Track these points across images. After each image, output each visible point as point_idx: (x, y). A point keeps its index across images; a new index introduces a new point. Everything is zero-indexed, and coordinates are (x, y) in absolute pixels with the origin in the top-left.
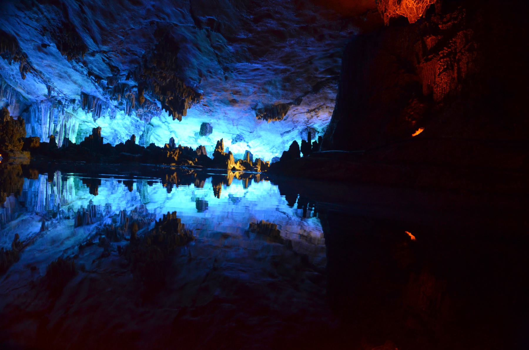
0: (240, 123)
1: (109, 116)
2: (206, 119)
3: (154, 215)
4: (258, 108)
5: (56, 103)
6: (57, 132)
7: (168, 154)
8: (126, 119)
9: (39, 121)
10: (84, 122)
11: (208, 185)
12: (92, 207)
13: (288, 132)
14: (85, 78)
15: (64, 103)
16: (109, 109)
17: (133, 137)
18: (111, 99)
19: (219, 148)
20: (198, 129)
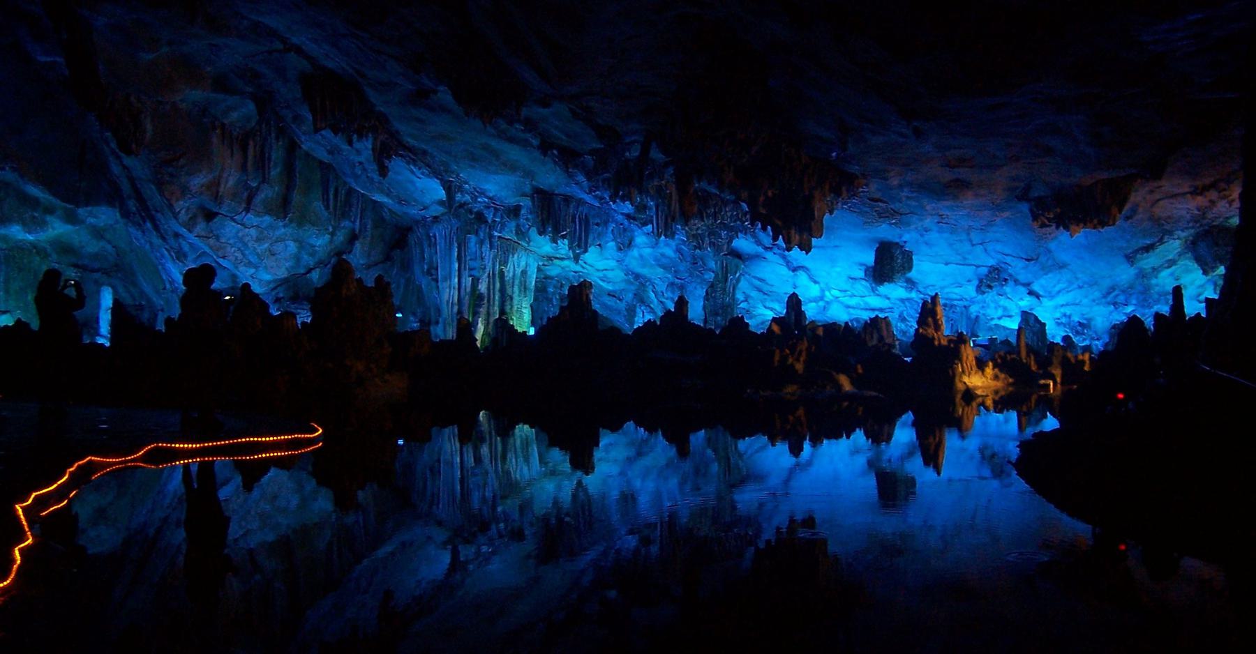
2: (886, 231)
4: (1035, 194)
5: (471, 220)
6: (480, 297)
7: (777, 357)
8: (661, 245)
9: (432, 271)
10: (550, 258)
11: (904, 434)
12: (583, 504)
13: (1148, 249)
14: (537, 154)
15: (490, 217)
16: (612, 226)
17: (682, 303)
18: (613, 198)
19: (928, 326)
20: (870, 259)
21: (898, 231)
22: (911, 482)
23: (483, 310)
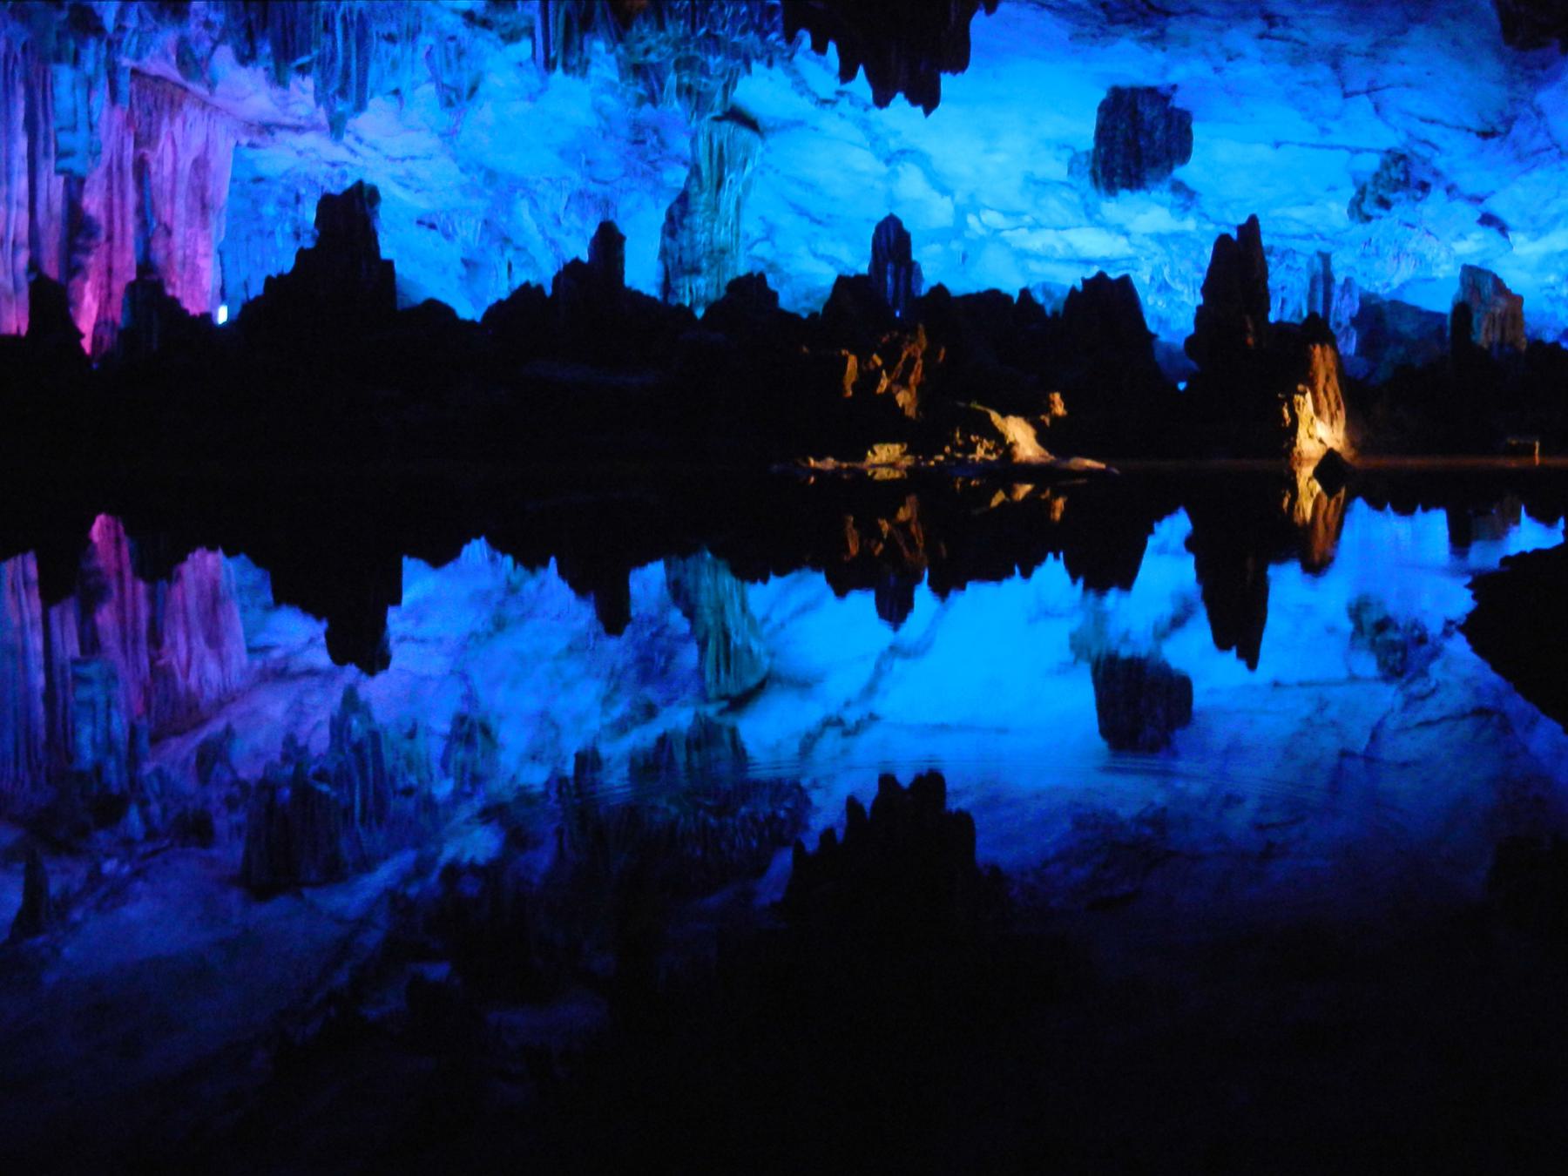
0: (1392, 72)
1: (435, 78)
2: (1132, 62)
3: (790, 794)
11: (1168, 566)
16: (426, 40)
17: (609, 241)
21: (1158, 57)
22: (1180, 687)
23: (94, 262)
